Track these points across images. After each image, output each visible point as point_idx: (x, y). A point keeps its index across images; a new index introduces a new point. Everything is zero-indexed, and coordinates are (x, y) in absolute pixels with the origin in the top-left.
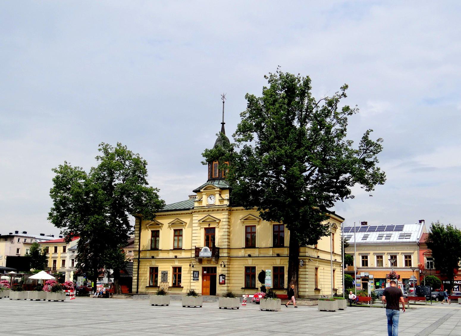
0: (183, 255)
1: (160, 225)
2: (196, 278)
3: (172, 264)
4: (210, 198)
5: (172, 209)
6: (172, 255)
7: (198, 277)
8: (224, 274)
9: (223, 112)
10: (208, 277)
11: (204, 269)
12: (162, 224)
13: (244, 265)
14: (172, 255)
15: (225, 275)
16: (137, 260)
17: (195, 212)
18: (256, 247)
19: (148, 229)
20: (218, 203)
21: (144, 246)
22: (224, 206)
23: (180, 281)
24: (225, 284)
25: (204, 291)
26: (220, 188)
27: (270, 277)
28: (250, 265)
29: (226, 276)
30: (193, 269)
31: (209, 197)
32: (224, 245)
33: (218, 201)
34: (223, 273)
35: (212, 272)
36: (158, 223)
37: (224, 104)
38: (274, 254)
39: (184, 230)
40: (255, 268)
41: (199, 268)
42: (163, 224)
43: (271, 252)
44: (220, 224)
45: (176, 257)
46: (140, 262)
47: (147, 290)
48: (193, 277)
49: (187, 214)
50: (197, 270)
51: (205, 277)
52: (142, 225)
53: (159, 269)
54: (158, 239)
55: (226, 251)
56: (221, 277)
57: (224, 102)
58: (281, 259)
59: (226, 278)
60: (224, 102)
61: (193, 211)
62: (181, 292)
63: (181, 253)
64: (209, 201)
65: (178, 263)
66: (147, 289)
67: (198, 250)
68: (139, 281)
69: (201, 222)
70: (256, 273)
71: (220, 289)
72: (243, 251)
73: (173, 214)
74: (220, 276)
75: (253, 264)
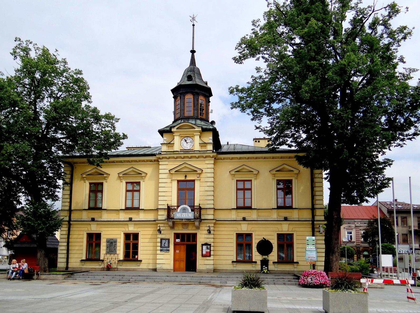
0: (142, 216)
1: (105, 176)
2: (166, 249)
3: (123, 229)
4: (186, 141)
5: (120, 154)
6: (123, 216)
7: (169, 247)
8: (209, 243)
9: (193, 38)
10: (183, 248)
11: (177, 236)
12: (107, 174)
13: (235, 231)
14: (123, 216)
15: (210, 245)
16: (67, 223)
17: (163, 158)
18: (253, 207)
19: (84, 180)
20: (197, 148)
21: (77, 203)
22: (208, 152)
23: (136, 253)
24: (210, 256)
25: (177, 266)
26: (202, 129)
27: (314, 248)
28: (245, 231)
29: (211, 245)
30: (160, 236)
31: (183, 140)
32: (208, 204)
33: (199, 145)
34: (208, 241)
35: (188, 240)
36: (102, 173)
37: (193, 27)
38: (278, 217)
39: (142, 184)
40: (292, 235)
41: (169, 234)
42: (110, 175)
43: (274, 215)
44: (203, 175)
45: (131, 220)
46: (71, 226)
47: (83, 265)
48: (161, 247)
49: (147, 161)
50: (167, 237)
51: (178, 246)
52: (74, 174)
53: (102, 236)
54: (99, 195)
55: (211, 212)
56: (205, 247)
57: (193, 25)
58: (289, 224)
59: (212, 248)
60: (193, 25)
61: (161, 156)
62: (138, 267)
63: (138, 214)
64: (183, 145)
65: (134, 228)
66: (83, 264)
67: (169, 209)
68: (70, 252)
69: (173, 172)
70: (197, 244)
71: (201, 263)
72: (234, 212)
73: (125, 161)
74: (203, 245)
75: (249, 230)
